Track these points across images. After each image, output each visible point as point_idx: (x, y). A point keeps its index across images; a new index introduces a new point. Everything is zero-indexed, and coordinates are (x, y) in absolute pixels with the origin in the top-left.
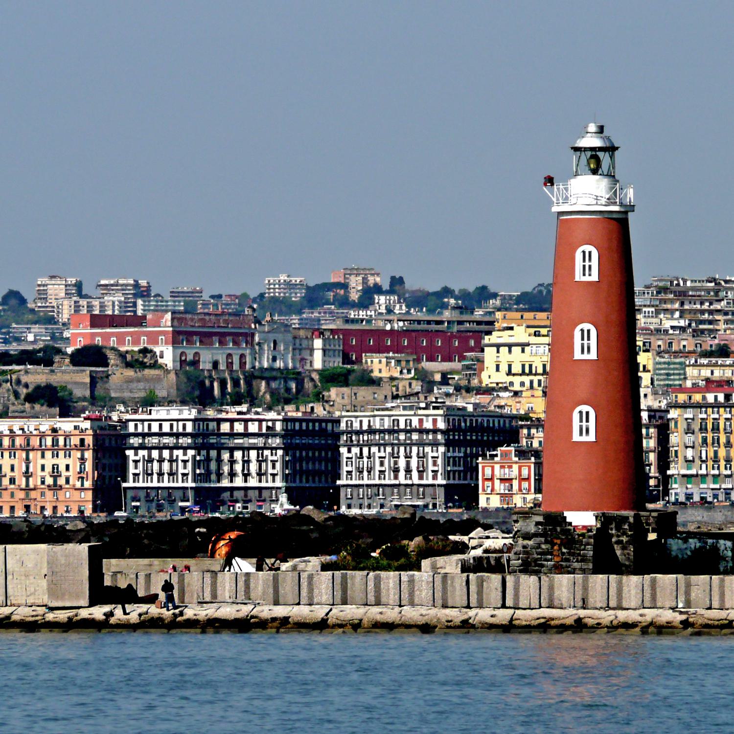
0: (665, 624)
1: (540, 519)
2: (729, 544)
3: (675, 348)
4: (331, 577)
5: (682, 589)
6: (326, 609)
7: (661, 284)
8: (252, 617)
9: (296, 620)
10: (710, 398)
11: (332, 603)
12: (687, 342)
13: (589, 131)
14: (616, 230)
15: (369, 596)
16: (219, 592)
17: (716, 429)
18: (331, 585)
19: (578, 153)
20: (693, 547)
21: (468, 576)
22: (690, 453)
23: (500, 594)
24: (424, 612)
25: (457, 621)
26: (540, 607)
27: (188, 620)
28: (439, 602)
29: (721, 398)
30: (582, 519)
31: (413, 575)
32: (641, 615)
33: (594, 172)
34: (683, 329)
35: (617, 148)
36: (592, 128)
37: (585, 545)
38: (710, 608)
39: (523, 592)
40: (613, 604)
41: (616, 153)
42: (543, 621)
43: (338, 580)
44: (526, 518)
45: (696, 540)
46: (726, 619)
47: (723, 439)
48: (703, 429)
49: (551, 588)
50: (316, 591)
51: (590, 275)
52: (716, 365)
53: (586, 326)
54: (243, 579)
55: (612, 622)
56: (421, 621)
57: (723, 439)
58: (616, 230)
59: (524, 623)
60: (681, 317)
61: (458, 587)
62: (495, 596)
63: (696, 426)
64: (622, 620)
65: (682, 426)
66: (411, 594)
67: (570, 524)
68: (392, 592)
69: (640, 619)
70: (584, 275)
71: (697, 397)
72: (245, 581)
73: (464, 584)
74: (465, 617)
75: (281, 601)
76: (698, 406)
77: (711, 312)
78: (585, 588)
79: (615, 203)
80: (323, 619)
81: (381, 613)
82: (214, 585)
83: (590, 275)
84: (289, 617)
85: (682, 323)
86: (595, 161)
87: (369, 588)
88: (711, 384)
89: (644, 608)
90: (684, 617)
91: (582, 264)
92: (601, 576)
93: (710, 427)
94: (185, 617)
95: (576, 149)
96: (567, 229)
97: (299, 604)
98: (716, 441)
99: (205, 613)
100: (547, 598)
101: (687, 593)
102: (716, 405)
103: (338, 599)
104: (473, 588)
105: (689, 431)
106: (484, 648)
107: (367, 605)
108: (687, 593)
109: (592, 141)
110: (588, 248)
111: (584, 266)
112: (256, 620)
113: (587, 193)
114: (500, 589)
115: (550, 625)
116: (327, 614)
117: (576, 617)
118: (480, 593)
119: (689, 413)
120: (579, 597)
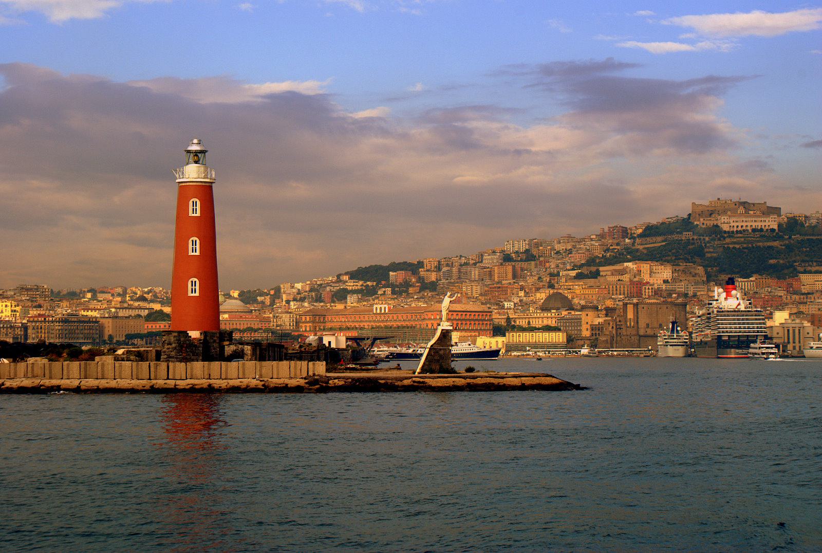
0: (255, 387)
1: (176, 334)
2: (249, 347)
3: (26, 305)
4: (79, 365)
5: (258, 368)
6: (78, 381)
7: (22, 286)
8: (41, 386)
9: (64, 387)
10: (40, 319)
11: (271, 377)
12: (30, 304)
13: (194, 142)
14: (206, 192)
15: (98, 374)
16: (18, 373)
17: (41, 328)
18: (79, 368)
19: (189, 154)
20: (232, 349)
21: (150, 363)
22: (34, 335)
23: (166, 372)
24: (130, 382)
25: (147, 387)
26: (187, 379)
27: (7, 388)
28: (134, 377)
29: (43, 319)
30: (194, 334)
31: (121, 363)
32: (241, 382)
33: (196, 162)
34: (28, 300)
35: (206, 151)
36: (195, 141)
37: (198, 347)
38: (272, 378)
39: (177, 372)
40: (223, 377)
41: (206, 153)
42: (191, 386)
43: (83, 366)
44: (169, 334)
45: (234, 346)
46: (284, 384)
47: (43, 331)
48: (38, 329)
49: (192, 369)
50: (71, 372)
51: (196, 213)
52: (38, 310)
53: (195, 238)
54: (31, 366)
55: (226, 386)
56: (130, 386)
57: (43, 331)
58: (206, 192)
59: (182, 387)
60: (27, 296)
61: (144, 369)
62: (163, 373)
63: (36, 328)
64: (232, 385)
65: (31, 328)
66: (120, 373)
67: (191, 337)
68: (110, 372)
69: (240, 384)
70: (193, 213)
71: (36, 319)
72: (32, 367)
73: (148, 367)
74: (151, 384)
75: (53, 376)
76: (36, 322)
77: (36, 295)
78: (209, 369)
79: (208, 178)
80: (78, 386)
81: (107, 383)
82: (15, 369)
83: (196, 213)
84: (60, 386)
85: (28, 298)
86: (197, 157)
87: (99, 370)
88: (40, 315)
89: (239, 378)
90: (263, 383)
91: (192, 208)
92: (217, 362)
93: (40, 328)
94: (5, 386)
95: (189, 152)
96: (185, 191)
97: (62, 379)
98: (41, 332)
99: (15, 384)
100: (190, 374)
101: (261, 371)
102: (41, 322)
103: (82, 376)
104: (152, 369)
105: (34, 329)
106: (402, 416)
107: (97, 379)
108: (261, 371)
109: (195, 148)
110: (195, 200)
111: (193, 209)
112: (44, 387)
113: (192, 173)
114: (166, 370)
115: (195, 388)
116: (79, 384)
117: (208, 383)
118: (156, 371)
119: (34, 324)
120: (206, 373)
